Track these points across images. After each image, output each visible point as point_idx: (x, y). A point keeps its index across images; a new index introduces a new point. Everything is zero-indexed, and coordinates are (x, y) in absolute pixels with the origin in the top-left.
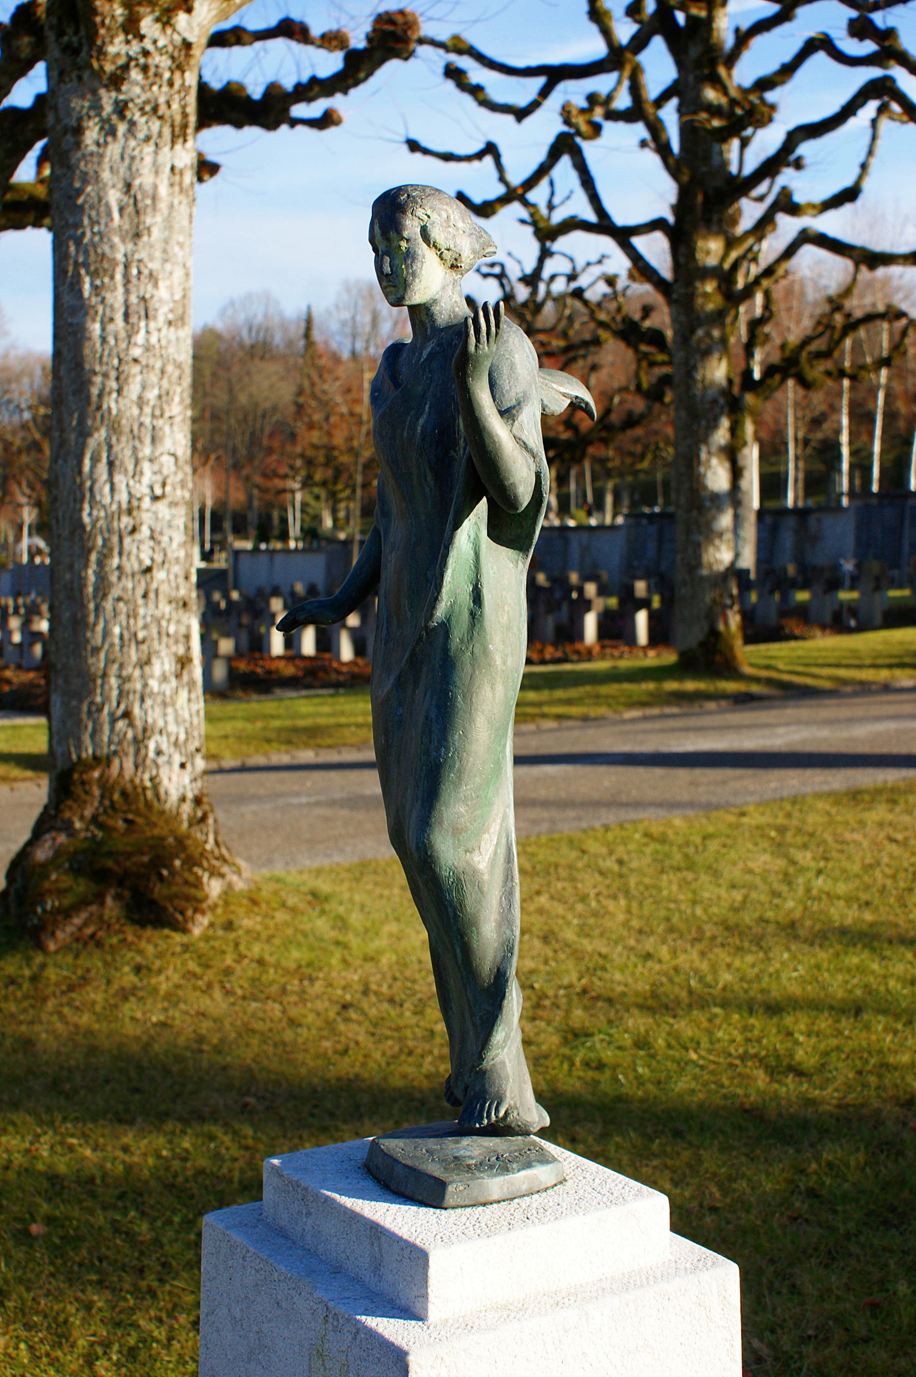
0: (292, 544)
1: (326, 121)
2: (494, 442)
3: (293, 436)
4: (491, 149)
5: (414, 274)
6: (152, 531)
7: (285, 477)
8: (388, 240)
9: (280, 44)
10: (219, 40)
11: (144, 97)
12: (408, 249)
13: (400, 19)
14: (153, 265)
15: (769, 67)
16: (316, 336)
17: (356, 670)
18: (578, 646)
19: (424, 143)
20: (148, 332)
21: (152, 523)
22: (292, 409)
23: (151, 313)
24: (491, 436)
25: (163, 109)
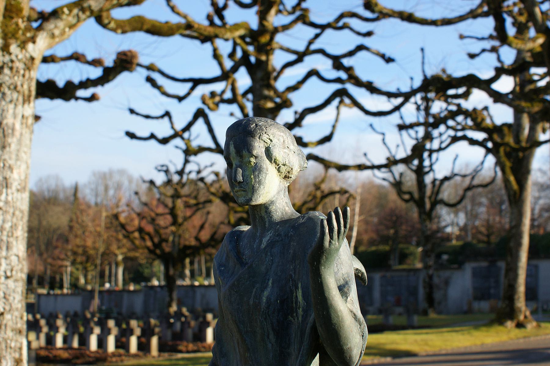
0: (65, 291)
1: (93, 98)
2: (338, 317)
3: (67, 241)
4: (167, 114)
5: (260, 183)
6: (5, 294)
7: (63, 260)
8: (241, 157)
9: (72, 63)
10: (46, 60)
11: (10, 82)
12: (256, 164)
13: (129, 54)
14: (11, 162)
15: (292, 82)
16: (80, 195)
17: (98, 355)
18: (204, 344)
19: (137, 110)
20: (7, 195)
21: (5, 290)
22: (67, 228)
23: (9, 185)
24: (336, 312)
25: (19, 88)
